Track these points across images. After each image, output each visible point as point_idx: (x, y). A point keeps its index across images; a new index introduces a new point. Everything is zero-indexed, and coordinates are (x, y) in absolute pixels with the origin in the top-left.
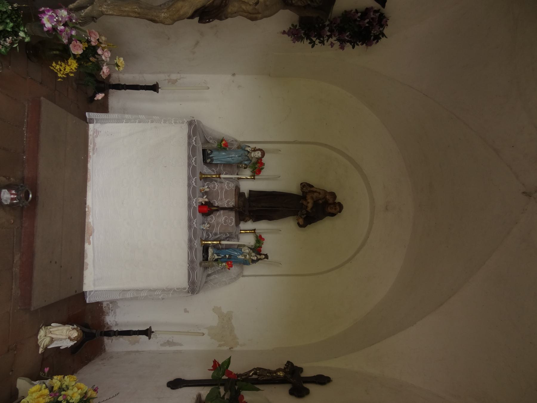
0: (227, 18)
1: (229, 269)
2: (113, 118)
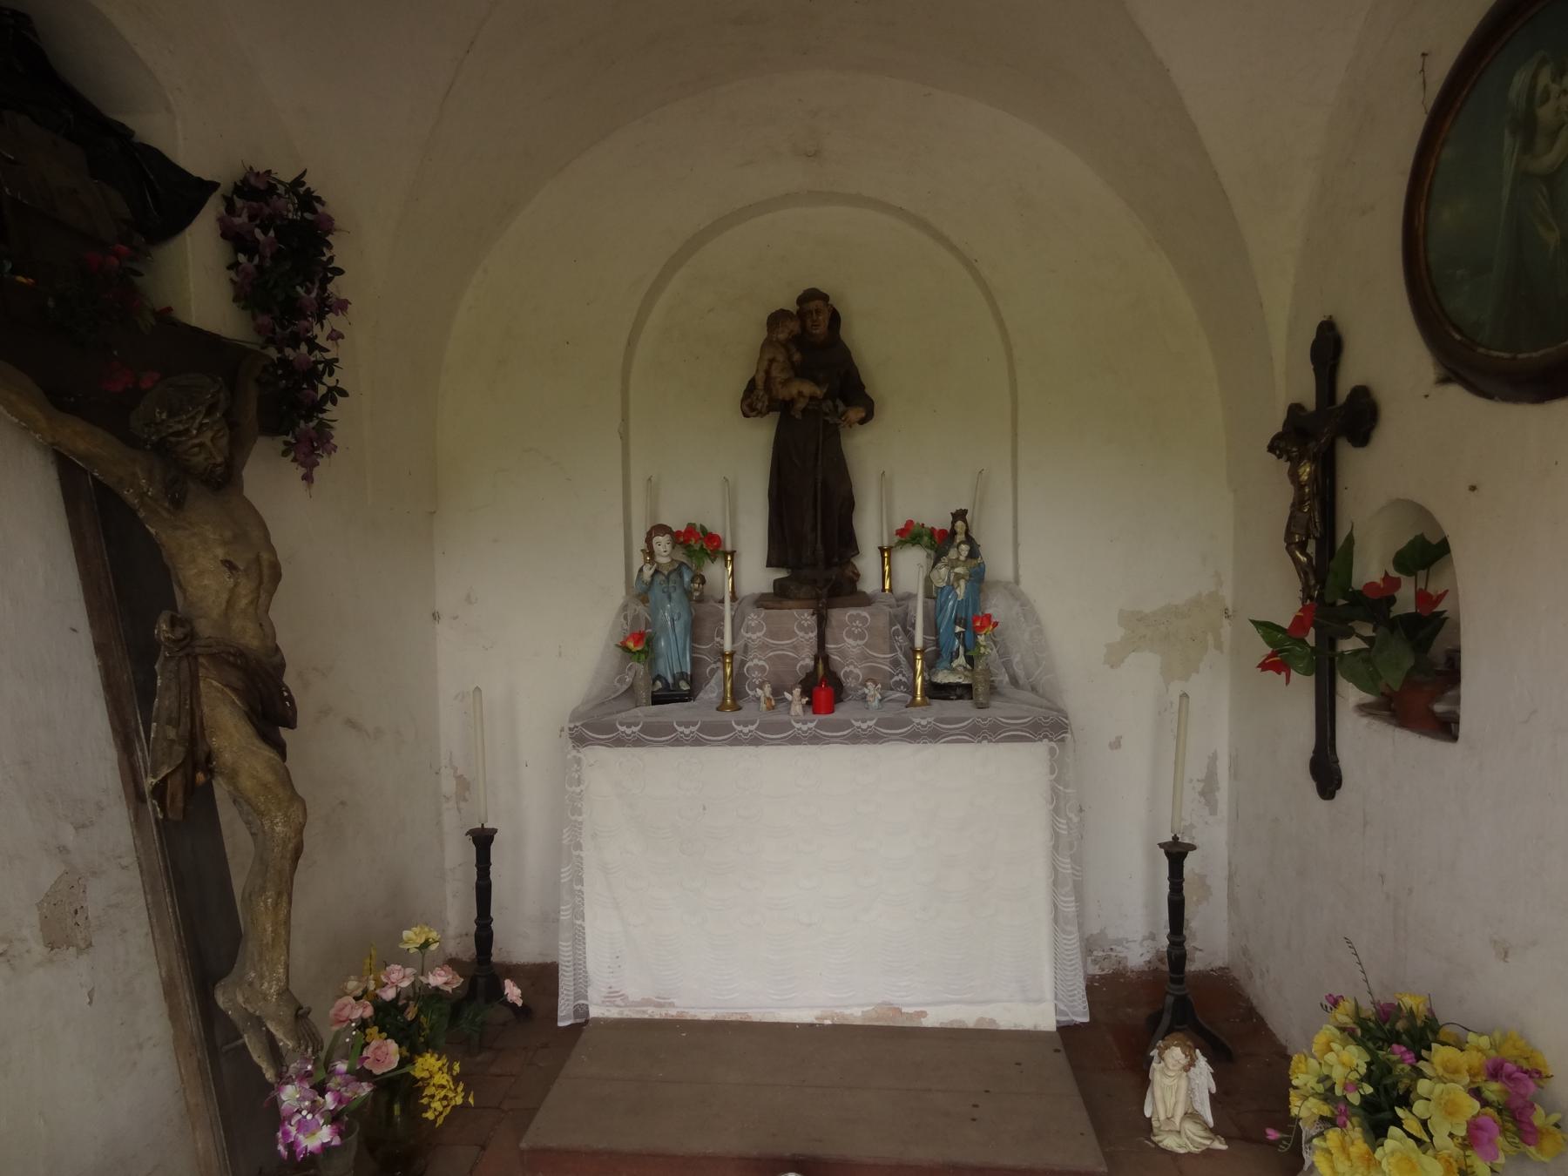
0: (277, 649)
1: (996, 624)
2: (570, 948)
